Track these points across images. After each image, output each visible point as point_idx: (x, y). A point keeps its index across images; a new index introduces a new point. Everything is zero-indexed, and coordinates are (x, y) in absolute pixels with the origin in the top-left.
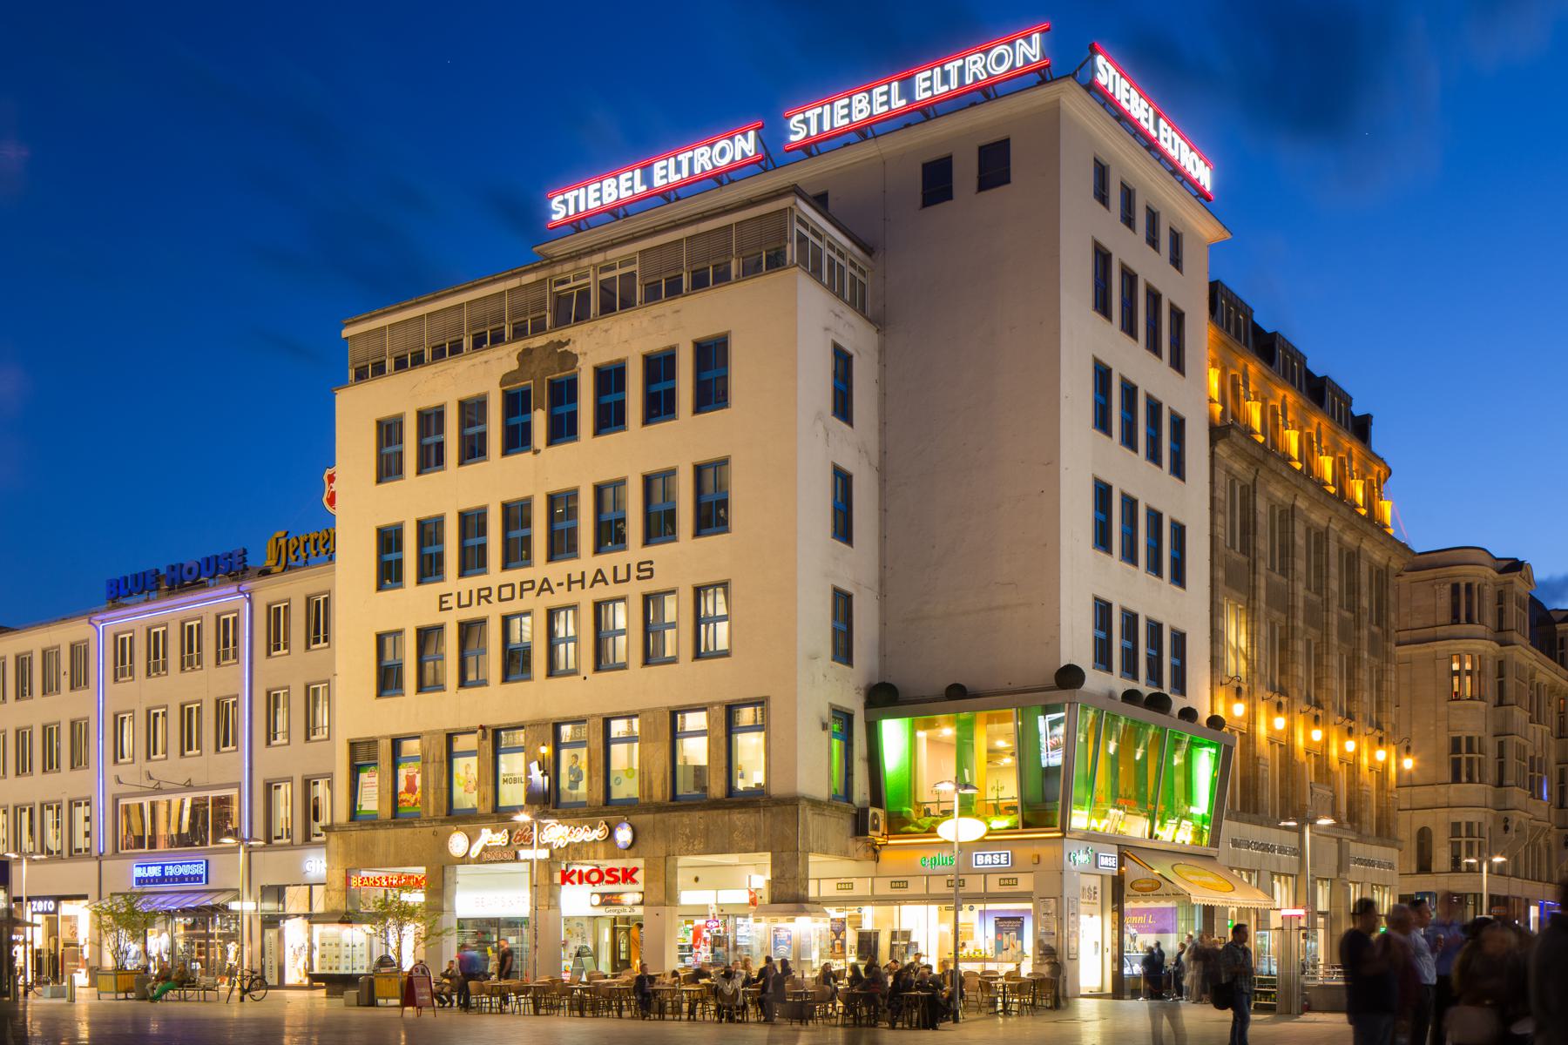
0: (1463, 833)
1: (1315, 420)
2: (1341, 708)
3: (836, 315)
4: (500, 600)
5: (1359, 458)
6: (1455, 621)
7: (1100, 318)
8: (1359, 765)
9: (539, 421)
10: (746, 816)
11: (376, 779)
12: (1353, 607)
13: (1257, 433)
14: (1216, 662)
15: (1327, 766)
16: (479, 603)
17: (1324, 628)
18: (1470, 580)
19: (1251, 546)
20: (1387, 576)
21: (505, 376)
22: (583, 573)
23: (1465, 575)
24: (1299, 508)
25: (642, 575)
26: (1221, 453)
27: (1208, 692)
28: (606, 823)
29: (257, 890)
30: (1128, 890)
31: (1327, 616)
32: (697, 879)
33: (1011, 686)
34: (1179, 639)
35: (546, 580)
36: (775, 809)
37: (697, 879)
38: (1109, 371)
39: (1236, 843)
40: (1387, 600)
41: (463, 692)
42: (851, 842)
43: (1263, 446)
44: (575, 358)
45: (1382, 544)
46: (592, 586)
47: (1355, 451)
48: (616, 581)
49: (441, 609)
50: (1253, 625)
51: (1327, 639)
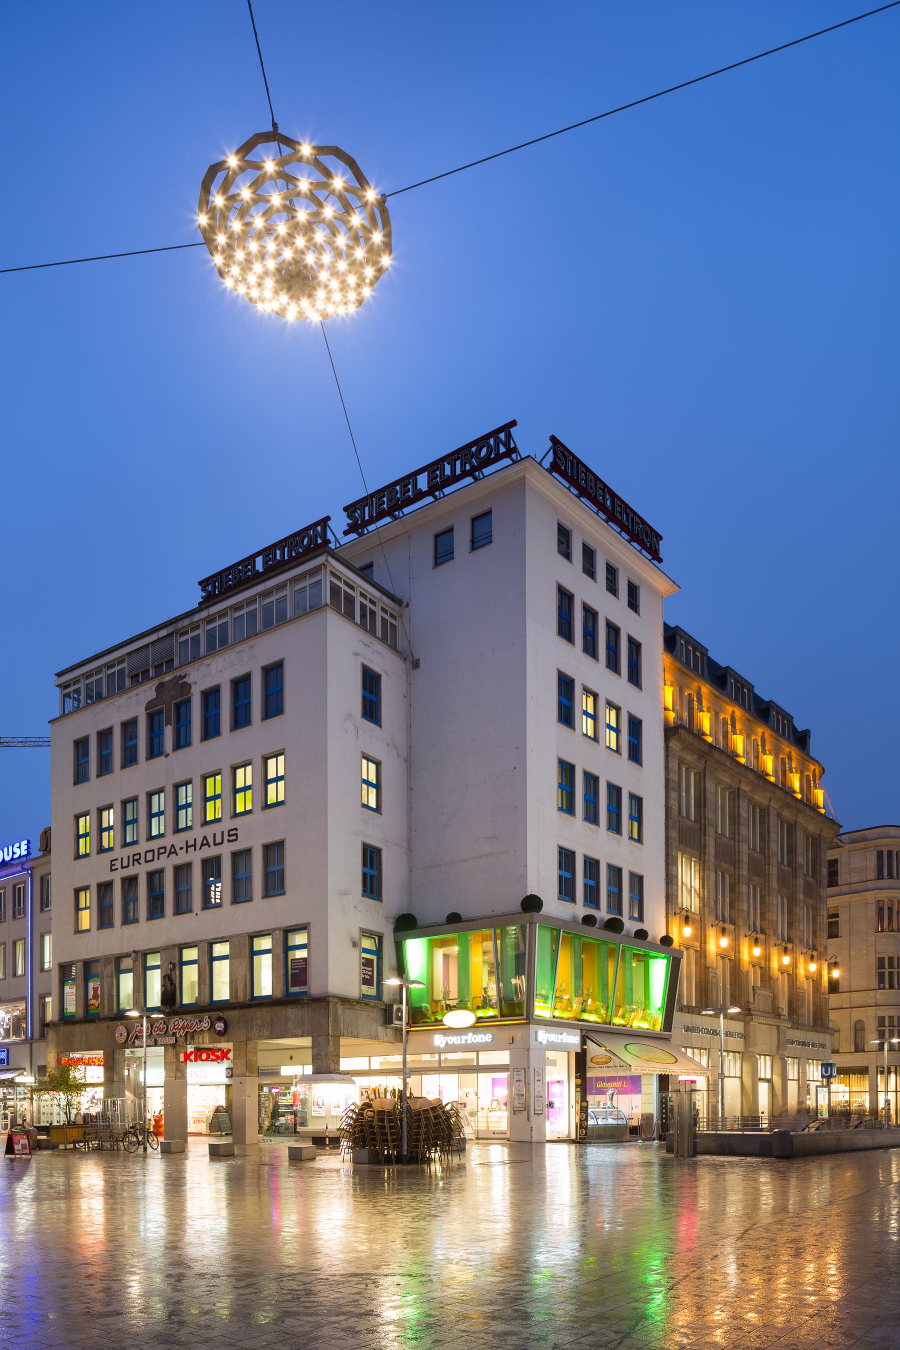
0: (887, 1024)
1: (760, 730)
2: (808, 942)
3: (365, 645)
4: (146, 862)
5: (797, 759)
6: (880, 877)
7: (563, 642)
8: (796, 975)
9: (169, 732)
10: (296, 1010)
11: (74, 990)
12: (792, 863)
13: (797, 793)
14: (670, 898)
15: (769, 974)
16: (133, 865)
17: (766, 877)
18: (890, 848)
19: (702, 816)
20: (820, 842)
21: (148, 703)
22: (195, 840)
23: (887, 845)
24: (744, 790)
25: (231, 838)
26: (673, 747)
27: (664, 920)
28: (209, 1018)
29: (35, 1068)
30: (589, 1064)
31: (769, 868)
32: (291, 1058)
33: (495, 913)
34: (638, 881)
35: (173, 846)
36: (314, 1005)
37: (291, 1058)
38: (572, 681)
39: (687, 1029)
40: (820, 859)
41: (126, 927)
42: (380, 1029)
43: (801, 801)
44: (189, 686)
45: (813, 818)
46: (200, 849)
47: (794, 754)
48: (215, 844)
49: (112, 870)
50: (704, 873)
51: (769, 885)
